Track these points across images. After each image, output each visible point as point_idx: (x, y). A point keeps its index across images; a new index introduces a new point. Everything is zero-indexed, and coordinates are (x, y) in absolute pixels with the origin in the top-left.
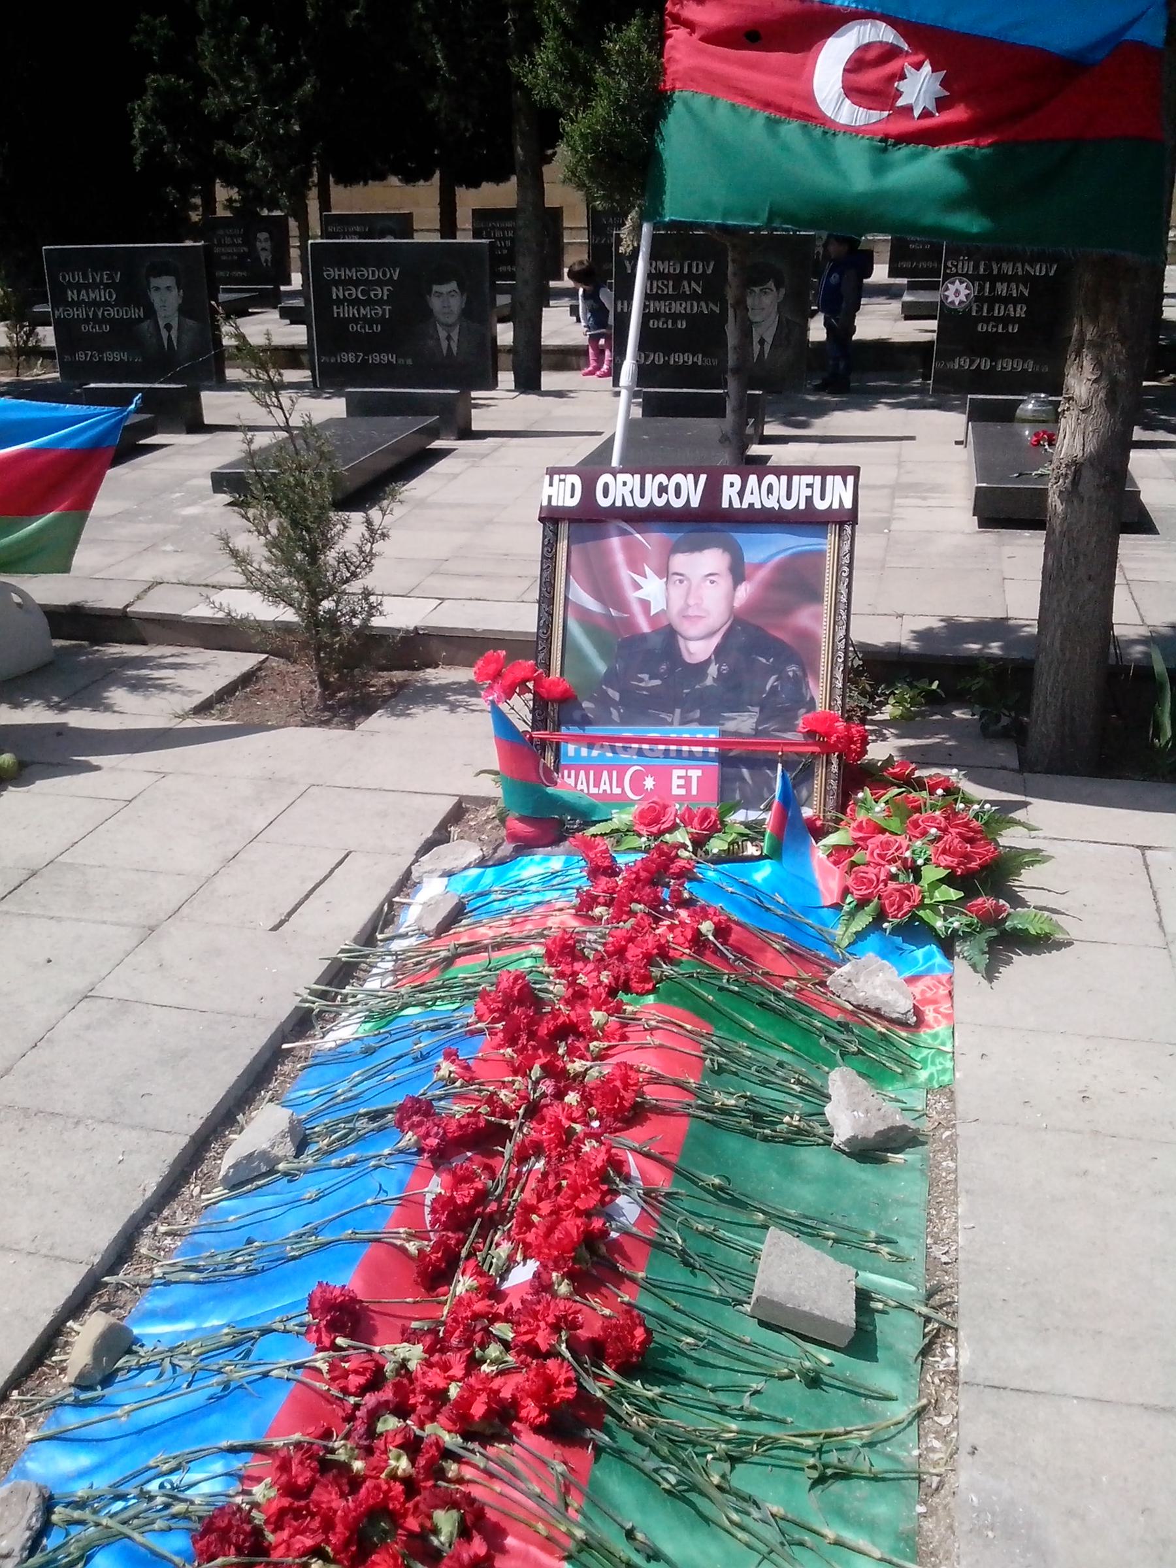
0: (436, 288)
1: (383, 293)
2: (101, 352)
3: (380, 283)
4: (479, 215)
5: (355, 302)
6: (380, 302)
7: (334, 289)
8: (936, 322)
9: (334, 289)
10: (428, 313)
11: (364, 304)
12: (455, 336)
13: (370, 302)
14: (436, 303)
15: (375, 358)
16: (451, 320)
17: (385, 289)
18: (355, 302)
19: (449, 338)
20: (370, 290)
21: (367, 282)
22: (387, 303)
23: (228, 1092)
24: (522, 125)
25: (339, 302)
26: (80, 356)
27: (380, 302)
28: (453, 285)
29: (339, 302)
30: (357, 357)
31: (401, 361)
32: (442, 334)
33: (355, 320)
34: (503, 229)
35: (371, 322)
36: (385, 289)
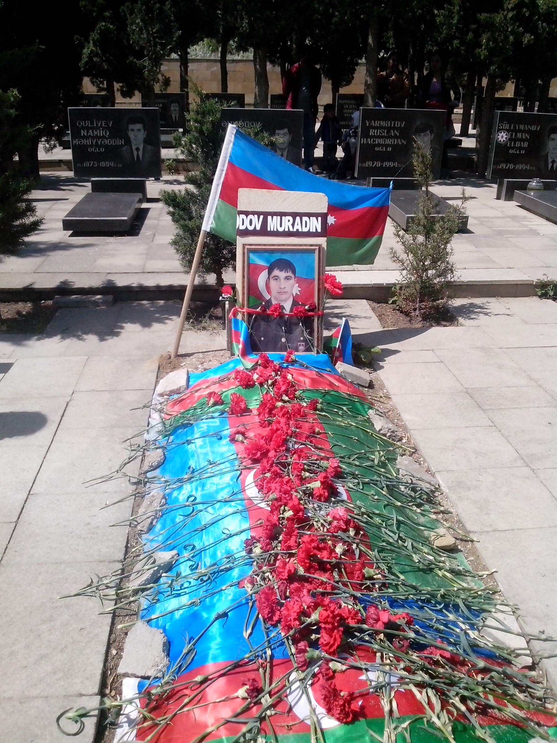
7: (82, 131)
9: (82, 131)
28: (286, 130)
35: (387, 146)
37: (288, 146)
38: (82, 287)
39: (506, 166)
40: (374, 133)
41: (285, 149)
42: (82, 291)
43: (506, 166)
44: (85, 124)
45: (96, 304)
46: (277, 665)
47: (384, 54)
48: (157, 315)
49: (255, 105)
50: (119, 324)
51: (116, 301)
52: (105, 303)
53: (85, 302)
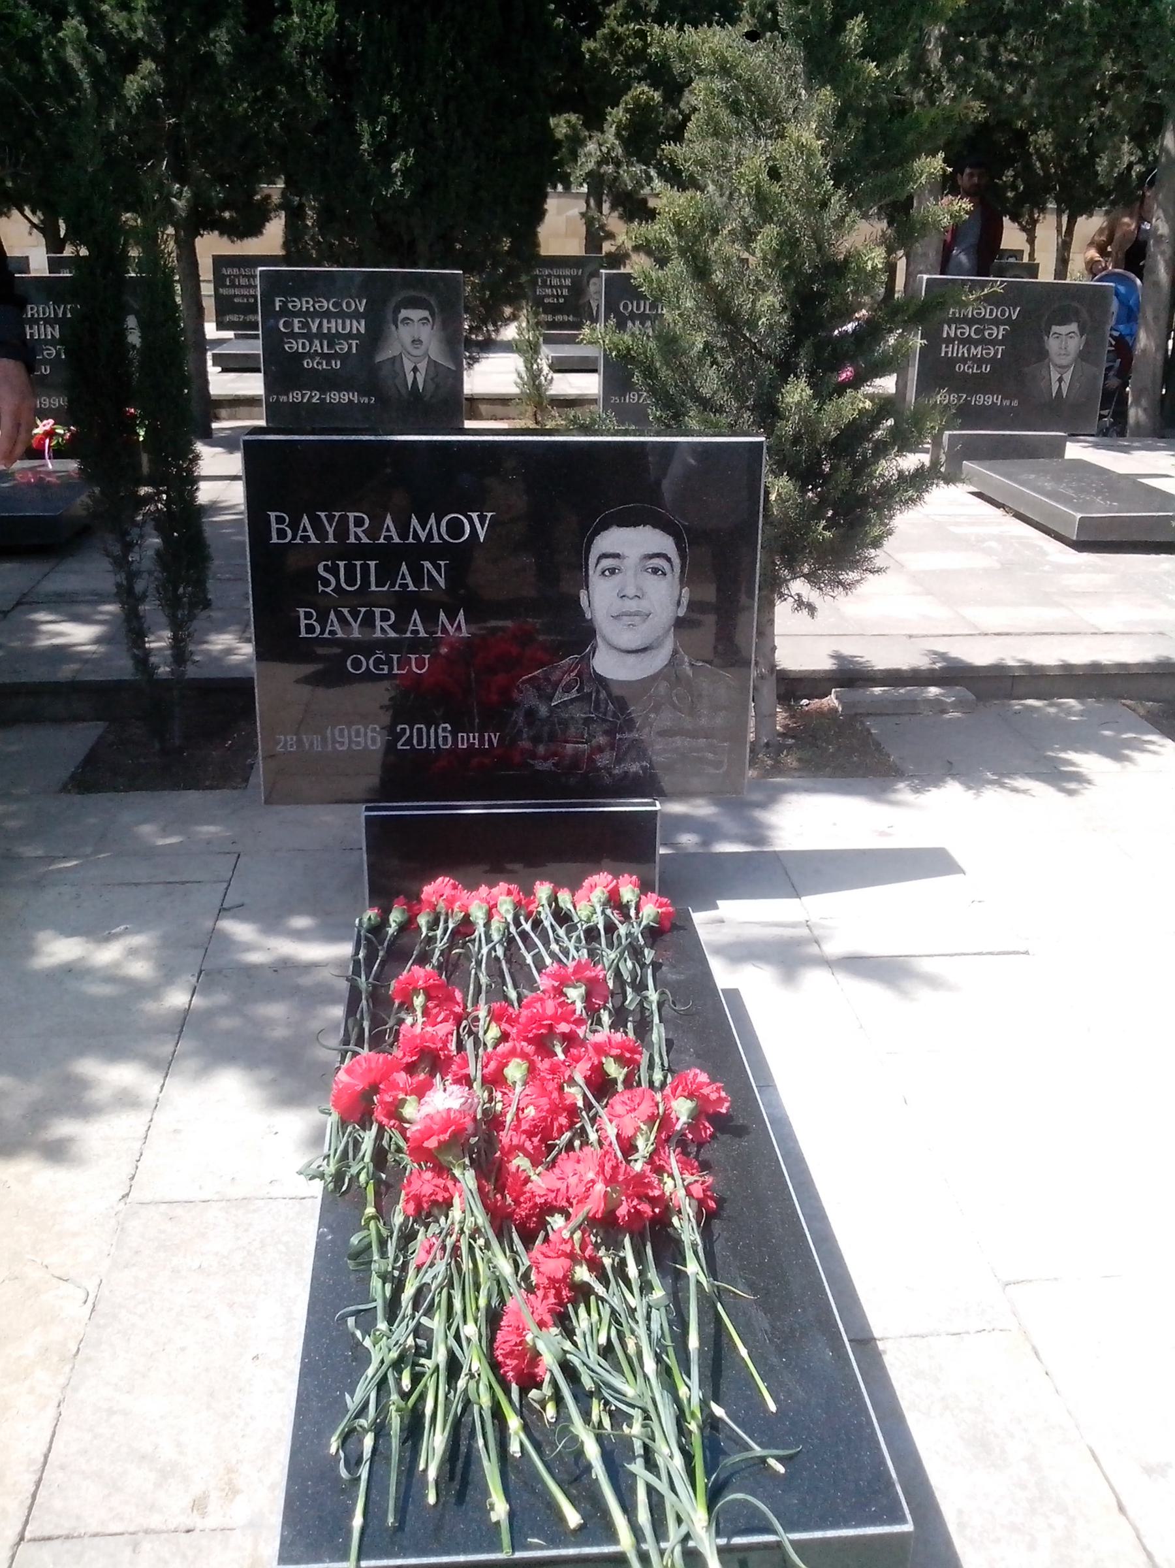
0: (1055, 329)
1: (999, 332)
2: (323, 392)
3: (997, 322)
4: (220, 262)
5: (967, 341)
6: (994, 342)
7: (946, 327)
8: (260, 377)
9: (946, 327)
10: (1043, 354)
11: (976, 343)
12: (1067, 377)
13: (983, 341)
14: (1052, 344)
15: (980, 400)
16: (1064, 361)
17: (1002, 328)
18: (967, 341)
19: (1060, 380)
20: (985, 329)
21: (982, 321)
22: (1001, 343)
23: (930, 1487)
24: (883, 178)
25: (949, 341)
26: (296, 397)
27: (994, 342)
28: (1073, 327)
29: (949, 341)
30: (370, 400)
31: (1007, 403)
32: (1055, 376)
33: (964, 360)
34: (559, 277)
35: (980, 362)
36: (1002, 328)
37: (1075, 360)
38: (895, 667)
39: (303, 397)
40: (38, 312)
41: (1068, 367)
42: (894, 678)
43: (303, 397)
44: (638, 308)
45: (938, 706)
46: (34, 1540)
47: (575, 142)
48: (1107, 733)
49: (286, 260)
50: (1127, 752)
51: (982, 697)
52: (959, 704)
53: (915, 701)
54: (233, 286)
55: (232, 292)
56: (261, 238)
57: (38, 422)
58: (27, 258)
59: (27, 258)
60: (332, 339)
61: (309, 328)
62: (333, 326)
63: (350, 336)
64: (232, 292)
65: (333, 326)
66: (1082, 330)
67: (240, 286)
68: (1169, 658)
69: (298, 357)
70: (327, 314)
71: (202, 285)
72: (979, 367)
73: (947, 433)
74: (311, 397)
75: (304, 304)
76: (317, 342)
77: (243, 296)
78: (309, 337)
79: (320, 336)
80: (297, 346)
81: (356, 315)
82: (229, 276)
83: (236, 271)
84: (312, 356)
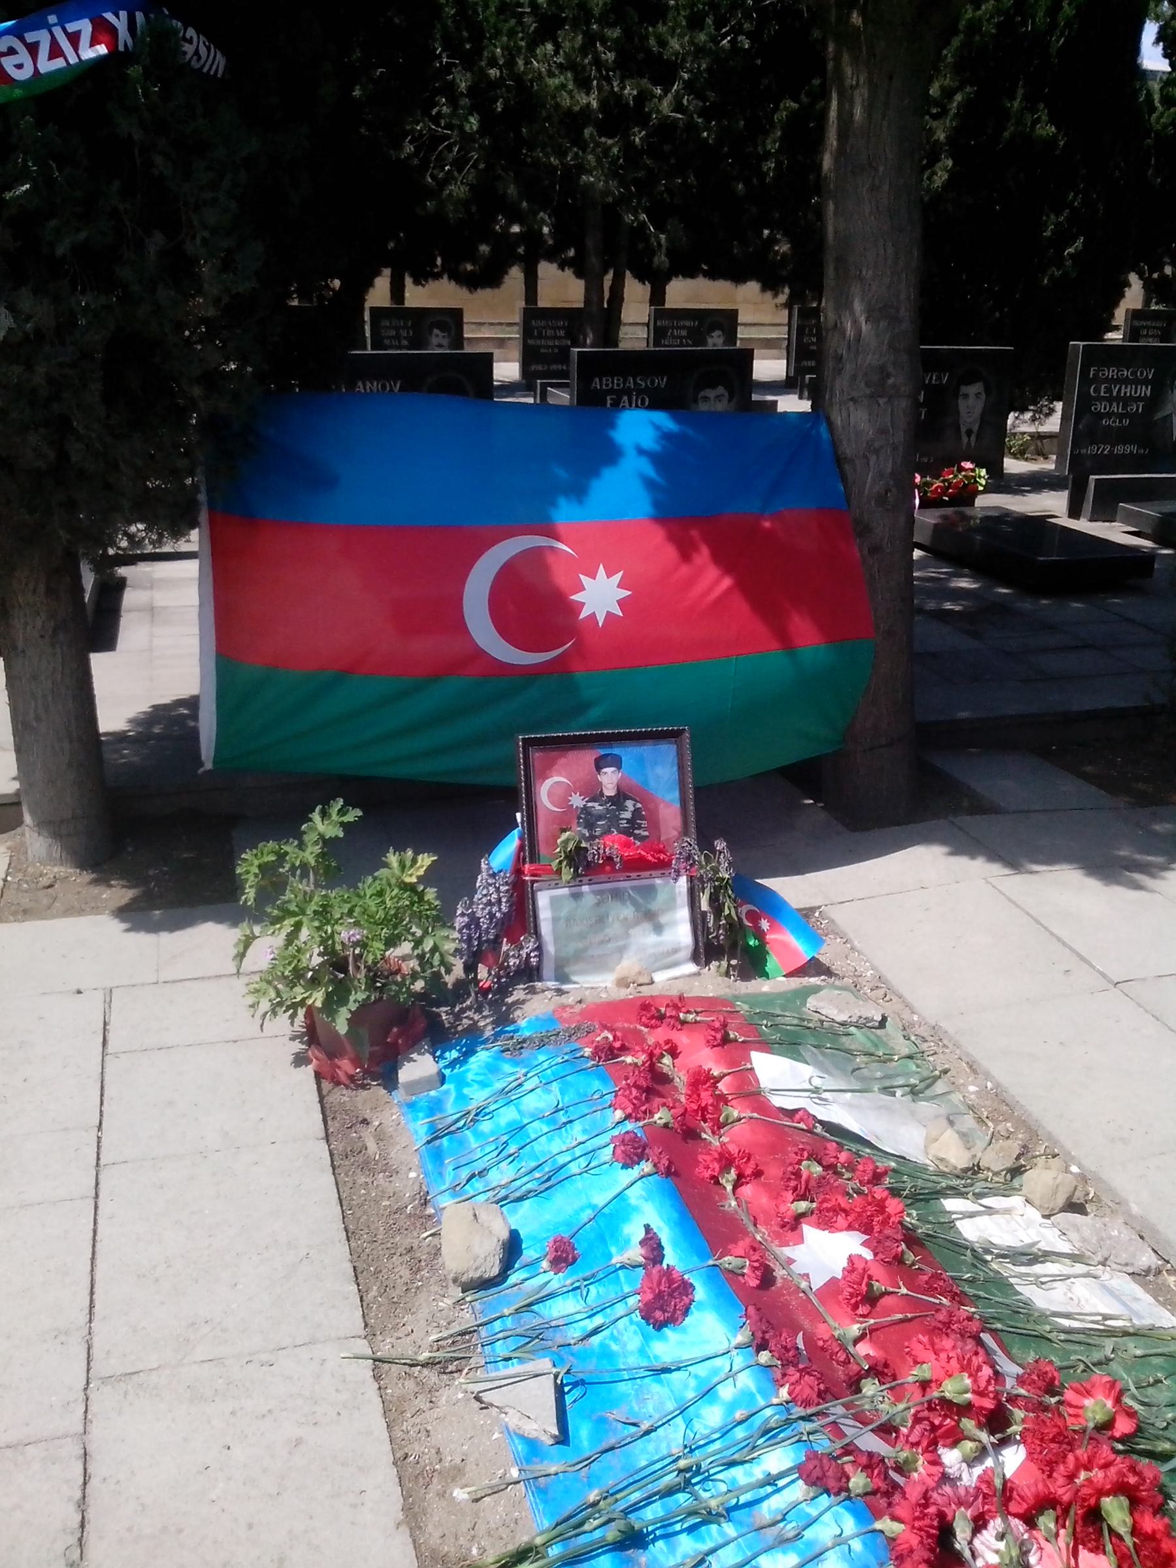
9: (1148, 393)
54: (540, 337)
55: (538, 342)
56: (496, 291)
57: (618, 577)
58: (737, 311)
59: (737, 311)
60: (1127, 401)
61: (1112, 392)
62: (1127, 391)
63: (1140, 399)
64: (538, 342)
65: (1127, 391)
66: (988, 391)
67: (546, 338)
68: (1106, 885)
69: (1100, 416)
70: (1126, 381)
71: (465, 327)
72: (1120, 422)
73: (1093, 477)
74: (1104, 450)
75: (1111, 373)
76: (1115, 404)
77: (549, 347)
78: (1110, 400)
79: (1118, 399)
80: (1101, 407)
81: (1146, 382)
82: (537, 328)
83: (543, 323)
84: (1109, 415)
